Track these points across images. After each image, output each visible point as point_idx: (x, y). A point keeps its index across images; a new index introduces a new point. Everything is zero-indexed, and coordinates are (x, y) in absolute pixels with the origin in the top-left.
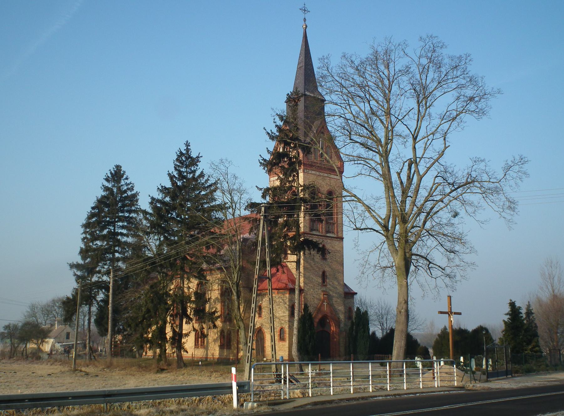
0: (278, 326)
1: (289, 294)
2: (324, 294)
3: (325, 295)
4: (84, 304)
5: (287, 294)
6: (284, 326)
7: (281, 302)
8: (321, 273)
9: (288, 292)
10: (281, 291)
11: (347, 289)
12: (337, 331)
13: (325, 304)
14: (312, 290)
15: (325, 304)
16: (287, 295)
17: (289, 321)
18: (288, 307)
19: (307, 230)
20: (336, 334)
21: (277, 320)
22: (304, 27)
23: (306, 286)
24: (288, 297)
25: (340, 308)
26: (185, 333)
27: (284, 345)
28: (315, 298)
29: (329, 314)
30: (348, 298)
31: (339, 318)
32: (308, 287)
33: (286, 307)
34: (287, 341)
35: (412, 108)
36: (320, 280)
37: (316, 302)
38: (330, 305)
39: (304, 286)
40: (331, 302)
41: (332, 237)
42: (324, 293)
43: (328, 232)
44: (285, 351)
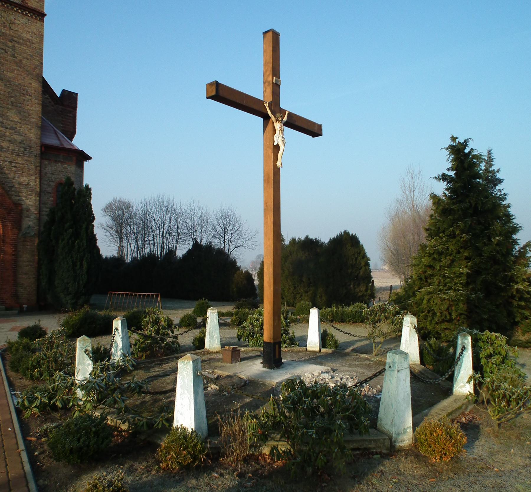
30: (56, 162)
31: (18, 205)
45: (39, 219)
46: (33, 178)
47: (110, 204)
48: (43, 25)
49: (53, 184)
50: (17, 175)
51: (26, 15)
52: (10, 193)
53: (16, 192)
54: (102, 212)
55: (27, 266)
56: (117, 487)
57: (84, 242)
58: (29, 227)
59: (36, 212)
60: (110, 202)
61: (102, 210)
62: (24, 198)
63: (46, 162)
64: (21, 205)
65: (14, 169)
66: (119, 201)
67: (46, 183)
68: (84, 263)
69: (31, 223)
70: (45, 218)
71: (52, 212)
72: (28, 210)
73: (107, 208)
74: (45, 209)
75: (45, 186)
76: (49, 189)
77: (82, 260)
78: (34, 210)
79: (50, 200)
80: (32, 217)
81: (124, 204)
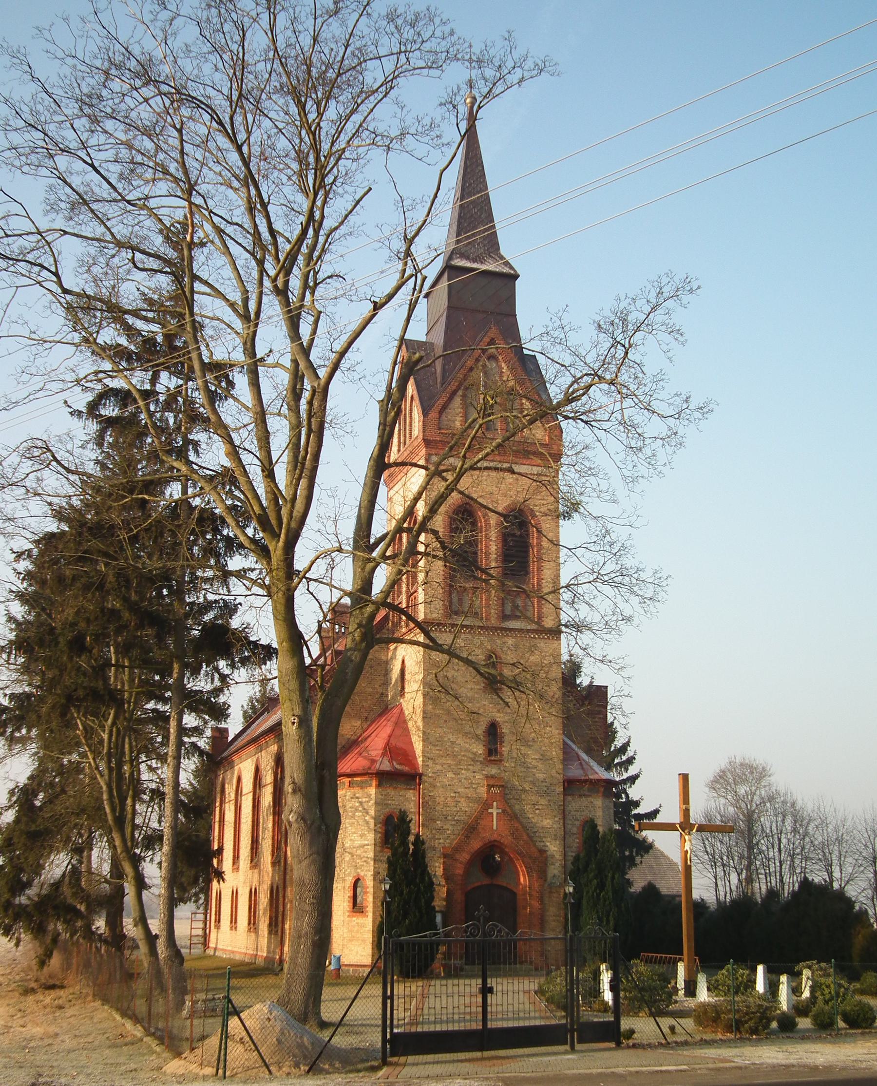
0: (349, 874)
1: (379, 786)
2: (489, 786)
3: (493, 786)
4: (650, 1010)
5: (370, 786)
6: (362, 874)
7: (357, 810)
8: (480, 730)
9: (374, 783)
10: (359, 779)
11: (581, 772)
12: (536, 885)
13: (494, 811)
14: (450, 775)
15: (494, 811)
16: (372, 791)
17: (375, 860)
18: (372, 822)
19: (437, 614)
20: (530, 895)
21: (347, 857)
22: (468, 100)
23: (431, 765)
24: (373, 796)
25: (547, 822)
26: (474, 982)
27: (363, 926)
28: (460, 797)
29: (507, 840)
30: (580, 796)
31: (542, 851)
32: (439, 767)
33: (367, 823)
34: (370, 915)
35: (366, 189)
36: (479, 749)
37: (464, 805)
38: (511, 816)
39: (425, 766)
40: (517, 807)
41: (521, 630)
42: (491, 783)
43: (505, 617)
44: (364, 941)
45: (565, 867)
46: (556, 819)
47: (724, 772)
48: (560, 644)
49: (577, 823)
50: (540, 819)
51: (543, 638)
52: (535, 839)
53: (539, 837)
54: (707, 789)
55: (554, 921)
56: (30, 612)
57: (610, 894)
58: (554, 876)
59: (561, 858)
60: (723, 767)
61: (707, 785)
62: (548, 844)
63: (569, 798)
64: (545, 851)
65: (537, 811)
66: (742, 764)
67: (570, 822)
68: (611, 918)
69: (556, 872)
70: (570, 866)
71: (577, 859)
72: (553, 856)
73: (715, 781)
74: (570, 854)
75: (570, 827)
76: (574, 830)
77: (608, 915)
78: (558, 856)
79: (575, 842)
80: (557, 865)
81: (752, 769)
